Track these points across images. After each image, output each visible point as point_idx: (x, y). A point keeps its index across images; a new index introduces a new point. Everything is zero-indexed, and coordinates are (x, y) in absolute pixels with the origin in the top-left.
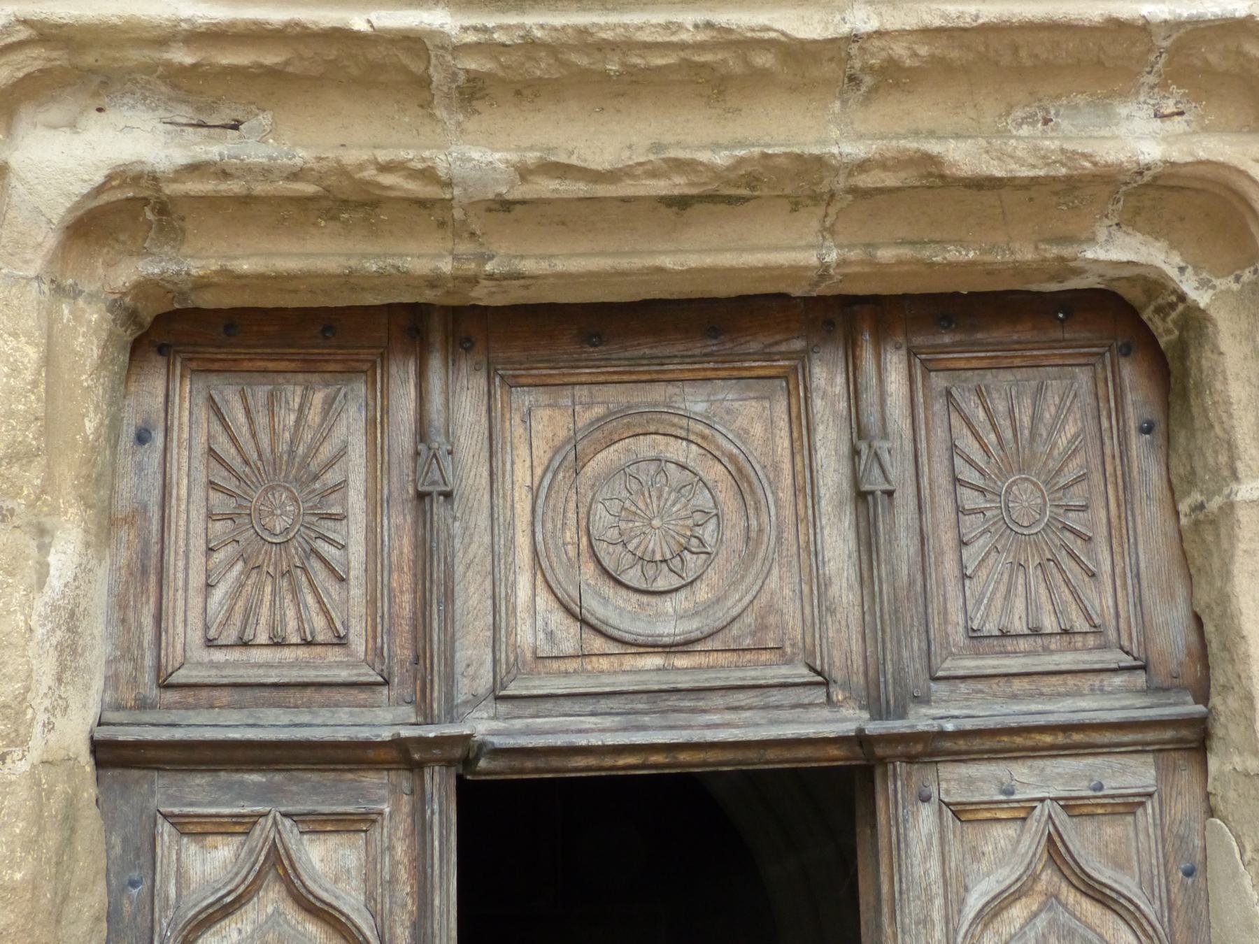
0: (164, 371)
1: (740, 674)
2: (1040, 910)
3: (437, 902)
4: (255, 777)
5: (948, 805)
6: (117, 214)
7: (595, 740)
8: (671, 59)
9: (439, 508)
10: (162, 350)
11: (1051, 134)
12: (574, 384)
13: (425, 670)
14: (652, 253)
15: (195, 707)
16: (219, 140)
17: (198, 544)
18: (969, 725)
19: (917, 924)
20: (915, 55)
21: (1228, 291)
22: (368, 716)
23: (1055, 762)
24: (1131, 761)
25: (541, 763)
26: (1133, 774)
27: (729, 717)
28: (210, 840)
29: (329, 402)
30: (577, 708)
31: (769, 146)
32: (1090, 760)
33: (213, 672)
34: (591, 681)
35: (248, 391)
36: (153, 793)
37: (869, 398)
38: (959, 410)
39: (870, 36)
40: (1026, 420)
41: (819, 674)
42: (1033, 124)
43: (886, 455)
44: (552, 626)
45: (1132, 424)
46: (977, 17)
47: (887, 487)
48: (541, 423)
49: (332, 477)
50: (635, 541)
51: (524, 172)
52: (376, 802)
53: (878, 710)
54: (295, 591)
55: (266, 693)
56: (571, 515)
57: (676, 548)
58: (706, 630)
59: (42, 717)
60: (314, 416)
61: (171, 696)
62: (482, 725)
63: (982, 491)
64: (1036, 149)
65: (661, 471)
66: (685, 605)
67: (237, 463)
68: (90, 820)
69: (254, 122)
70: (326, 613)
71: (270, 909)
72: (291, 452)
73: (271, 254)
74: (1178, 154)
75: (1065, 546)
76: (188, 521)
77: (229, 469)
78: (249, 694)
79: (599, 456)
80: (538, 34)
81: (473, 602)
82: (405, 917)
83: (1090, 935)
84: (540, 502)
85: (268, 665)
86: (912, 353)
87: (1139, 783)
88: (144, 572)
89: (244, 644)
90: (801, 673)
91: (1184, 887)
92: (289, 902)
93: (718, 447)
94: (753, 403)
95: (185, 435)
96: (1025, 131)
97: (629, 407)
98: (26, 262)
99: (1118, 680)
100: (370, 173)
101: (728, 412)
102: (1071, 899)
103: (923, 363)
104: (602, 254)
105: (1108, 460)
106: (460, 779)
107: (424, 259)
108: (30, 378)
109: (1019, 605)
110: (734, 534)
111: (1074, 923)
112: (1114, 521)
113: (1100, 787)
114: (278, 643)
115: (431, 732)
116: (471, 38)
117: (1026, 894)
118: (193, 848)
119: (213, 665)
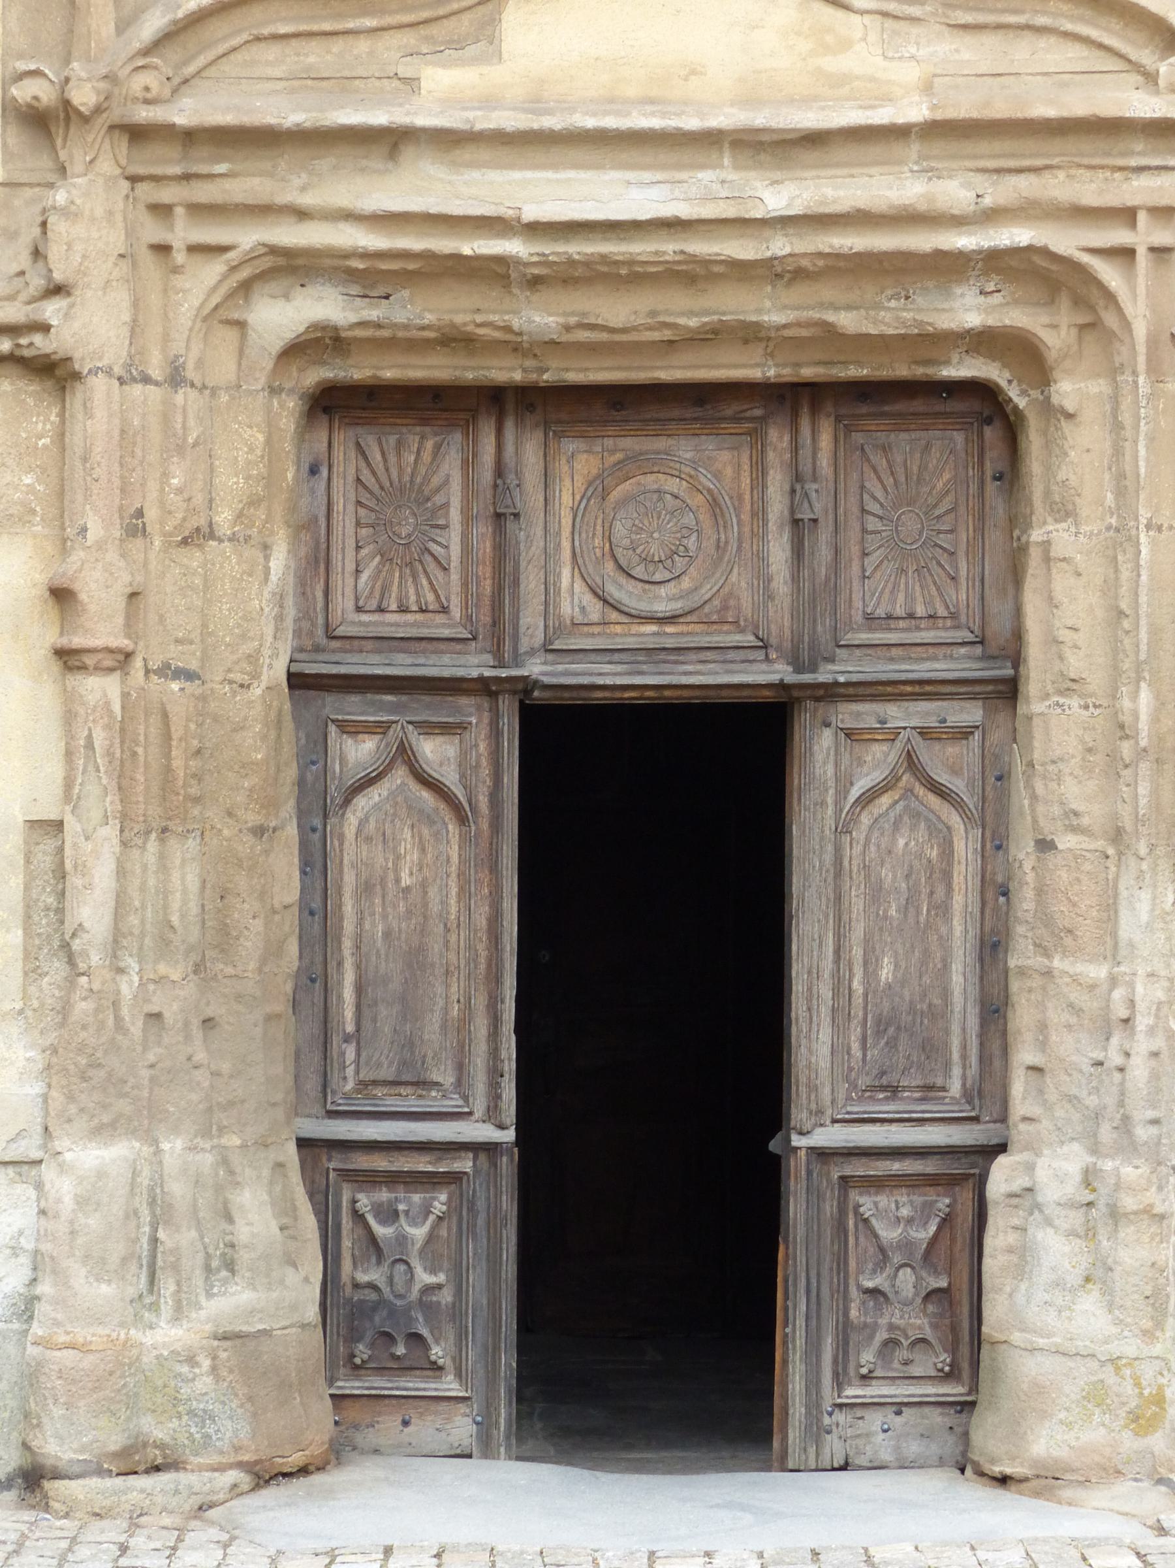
0: (327, 425)
1: (708, 639)
2: (900, 799)
3: (505, 780)
4: (389, 698)
5: (842, 729)
6: (321, 342)
7: (609, 681)
8: (660, 268)
9: (510, 525)
10: (326, 410)
11: (910, 306)
12: (603, 436)
13: (499, 631)
14: (653, 368)
15: (350, 651)
16: (377, 306)
17: (351, 543)
18: (855, 678)
19: (816, 804)
20: (815, 265)
21: (1037, 399)
22: (462, 660)
23: (915, 703)
24: (968, 705)
25: (574, 694)
26: (969, 713)
27: (700, 667)
28: (361, 736)
29: (438, 447)
30: (599, 659)
31: (724, 314)
32: (939, 703)
33: (362, 629)
34: (609, 641)
35: (383, 440)
36: (324, 706)
37: (805, 453)
38: (868, 460)
39: (785, 256)
40: (915, 469)
41: (762, 640)
42: (898, 299)
43: (814, 495)
44: (585, 603)
45: (989, 474)
46: (851, 248)
47: (812, 516)
48: (580, 462)
49: (439, 499)
50: (642, 547)
51: (568, 328)
52: (467, 716)
53: (798, 670)
54: (415, 577)
55: (395, 643)
56: (599, 528)
57: (669, 553)
58: (687, 609)
59: (267, 661)
60: (426, 456)
61: (335, 644)
62: (535, 668)
63: (881, 518)
64: (898, 318)
65: (660, 499)
66: (674, 591)
67: (376, 488)
68: (289, 724)
69: (399, 295)
70: (435, 591)
71: (399, 782)
72: (412, 482)
73: (404, 367)
75: (934, 558)
76: (344, 526)
77: (371, 493)
78: (385, 644)
79: (619, 488)
80: (577, 257)
81: (532, 586)
82: (485, 789)
83: (931, 816)
84: (578, 519)
85: (397, 625)
86: (838, 419)
87: (970, 719)
88: (317, 561)
90: (750, 639)
91: (995, 788)
92: (411, 777)
93: (700, 483)
94: (726, 452)
95: (341, 469)
96: (893, 304)
97: (641, 454)
98: (256, 379)
99: (963, 650)
100: (470, 328)
101: (709, 458)
102: (921, 793)
103: (845, 427)
104: (619, 368)
105: (971, 498)
106: (521, 702)
107: (506, 371)
108: (259, 454)
109: (901, 597)
110: (709, 545)
111: (921, 808)
112: (971, 540)
113: (945, 721)
114: (403, 610)
115: (504, 673)
116: (535, 259)
117: (890, 788)
118: (350, 741)
119: (361, 624)
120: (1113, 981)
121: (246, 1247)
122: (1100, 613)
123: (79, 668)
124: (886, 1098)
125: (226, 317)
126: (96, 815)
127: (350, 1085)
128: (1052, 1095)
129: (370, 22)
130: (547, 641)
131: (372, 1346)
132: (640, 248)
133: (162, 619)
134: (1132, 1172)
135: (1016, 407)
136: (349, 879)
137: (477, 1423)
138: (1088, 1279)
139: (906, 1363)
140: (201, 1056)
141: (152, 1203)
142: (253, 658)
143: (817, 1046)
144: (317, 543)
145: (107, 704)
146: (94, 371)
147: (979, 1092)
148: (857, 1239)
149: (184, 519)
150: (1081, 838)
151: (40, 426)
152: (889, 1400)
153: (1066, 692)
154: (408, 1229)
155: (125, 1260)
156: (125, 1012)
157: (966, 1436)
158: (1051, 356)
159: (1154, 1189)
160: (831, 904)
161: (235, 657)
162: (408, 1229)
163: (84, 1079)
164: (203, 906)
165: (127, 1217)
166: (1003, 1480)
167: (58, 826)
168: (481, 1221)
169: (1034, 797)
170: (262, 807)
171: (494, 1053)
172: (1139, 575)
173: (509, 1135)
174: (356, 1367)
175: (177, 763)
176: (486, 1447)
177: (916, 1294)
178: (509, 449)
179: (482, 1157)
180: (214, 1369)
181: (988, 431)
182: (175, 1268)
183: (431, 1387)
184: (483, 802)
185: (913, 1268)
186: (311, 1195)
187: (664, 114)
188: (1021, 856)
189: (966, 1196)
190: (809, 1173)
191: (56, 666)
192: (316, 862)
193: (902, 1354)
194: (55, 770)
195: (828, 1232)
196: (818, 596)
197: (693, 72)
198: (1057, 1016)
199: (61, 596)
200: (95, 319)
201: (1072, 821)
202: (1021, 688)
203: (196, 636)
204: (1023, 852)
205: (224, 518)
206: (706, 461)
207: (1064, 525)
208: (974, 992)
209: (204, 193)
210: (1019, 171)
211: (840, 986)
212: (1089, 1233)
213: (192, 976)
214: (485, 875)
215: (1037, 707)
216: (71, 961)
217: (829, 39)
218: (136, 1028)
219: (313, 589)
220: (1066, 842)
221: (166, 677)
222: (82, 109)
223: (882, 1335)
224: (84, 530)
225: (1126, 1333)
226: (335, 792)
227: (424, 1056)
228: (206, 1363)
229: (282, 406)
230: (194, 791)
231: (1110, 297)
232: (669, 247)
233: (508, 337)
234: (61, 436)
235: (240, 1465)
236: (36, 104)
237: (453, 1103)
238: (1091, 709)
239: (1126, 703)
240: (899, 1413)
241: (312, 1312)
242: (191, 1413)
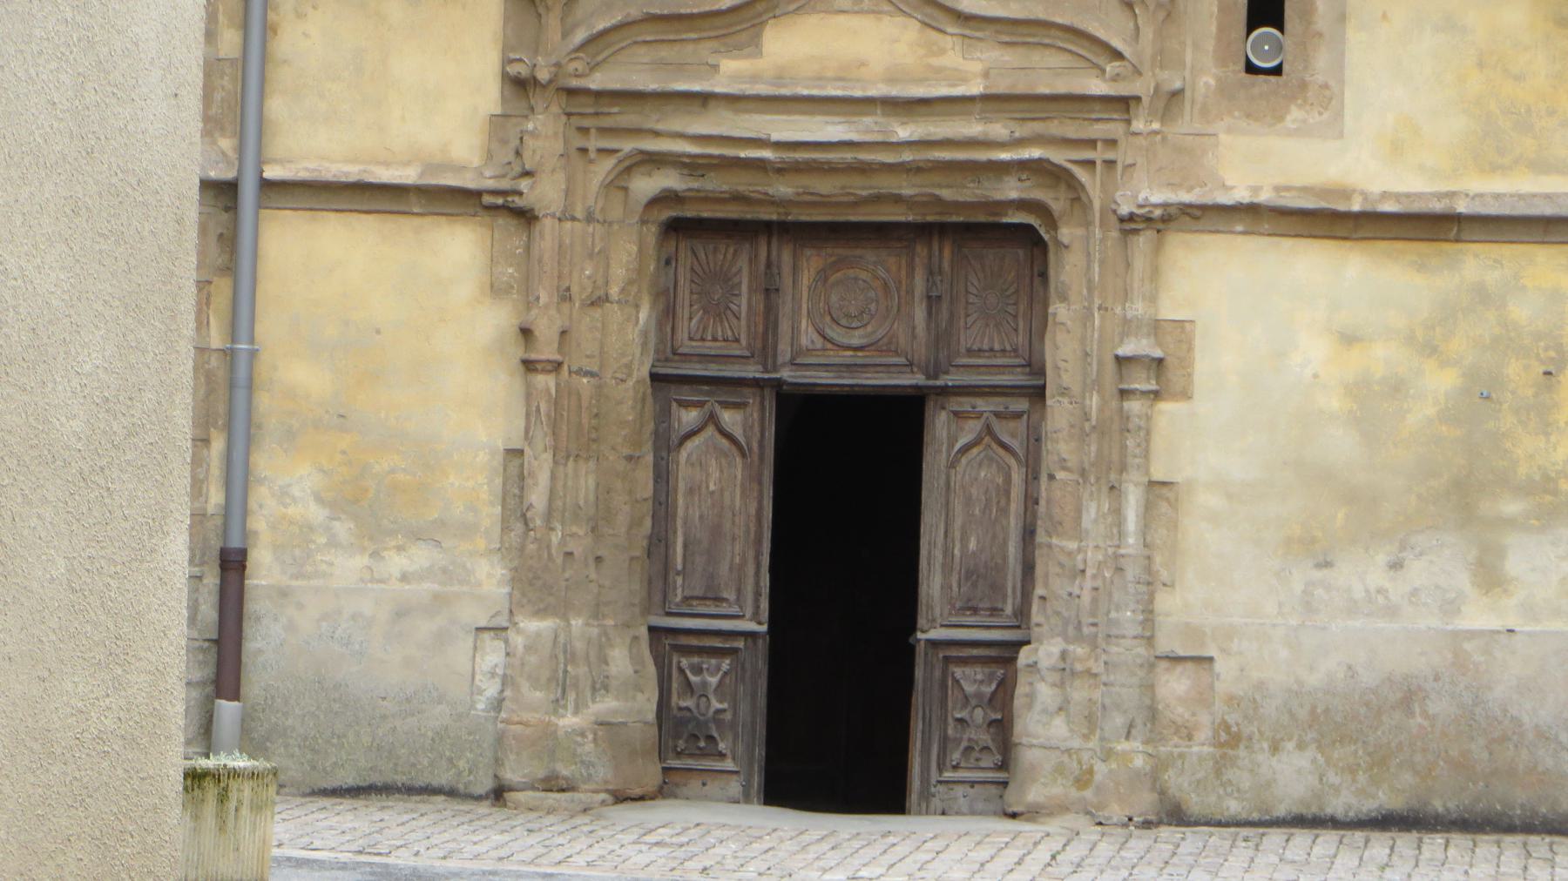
13: (765, 350)
17: (687, 303)
26: (1021, 405)
37: (935, 260)
48: (812, 262)
53: (928, 378)
60: (729, 256)
62: (786, 374)
68: (650, 400)
74: (1024, 195)
89: (703, 339)
90: (902, 360)
114: (715, 339)
115: (766, 376)
120: (1079, 550)
125: (617, 184)
126: (540, 446)
127: (678, 599)
128: (1049, 611)
129: (693, 36)
130: (793, 358)
134: (1079, 650)
136: (682, 486)
138: (1060, 709)
140: (593, 576)
141: (565, 652)
142: (629, 366)
143: (933, 585)
146: (545, 216)
153: (1062, 394)
155: (549, 680)
156: (554, 551)
158: (1056, 215)
163: (531, 584)
167: (521, 452)
168: (748, 674)
171: (757, 583)
173: (764, 628)
175: (585, 421)
176: (746, 798)
178: (774, 253)
180: (595, 740)
182: (576, 686)
183: (718, 765)
184: (755, 445)
187: (844, 88)
191: (522, 368)
192: (663, 475)
193: (975, 754)
194: (521, 423)
195: (936, 687)
196: (941, 338)
199: (526, 333)
203: (597, 353)
204: (1044, 478)
205: (614, 291)
206: (877, 265)
208: (1020, 556)
209: (607, 122)
210: (1033, 119)
211: (948, 552)
212: (1061, 685)
214: (755, 486)
216: (526, 524)
218: (559, 561)
220: (1060, 475)
223: (964, 744)
224: (538, 298)
226: (675, 439)
228: (591, 737)
230: (594, 436)
231: (1083, 186)
232: (849, 156)
234: (528, 249)
235: (607, 791)
237: (735, 610)
241: (651, 716)
242: (582, 762)
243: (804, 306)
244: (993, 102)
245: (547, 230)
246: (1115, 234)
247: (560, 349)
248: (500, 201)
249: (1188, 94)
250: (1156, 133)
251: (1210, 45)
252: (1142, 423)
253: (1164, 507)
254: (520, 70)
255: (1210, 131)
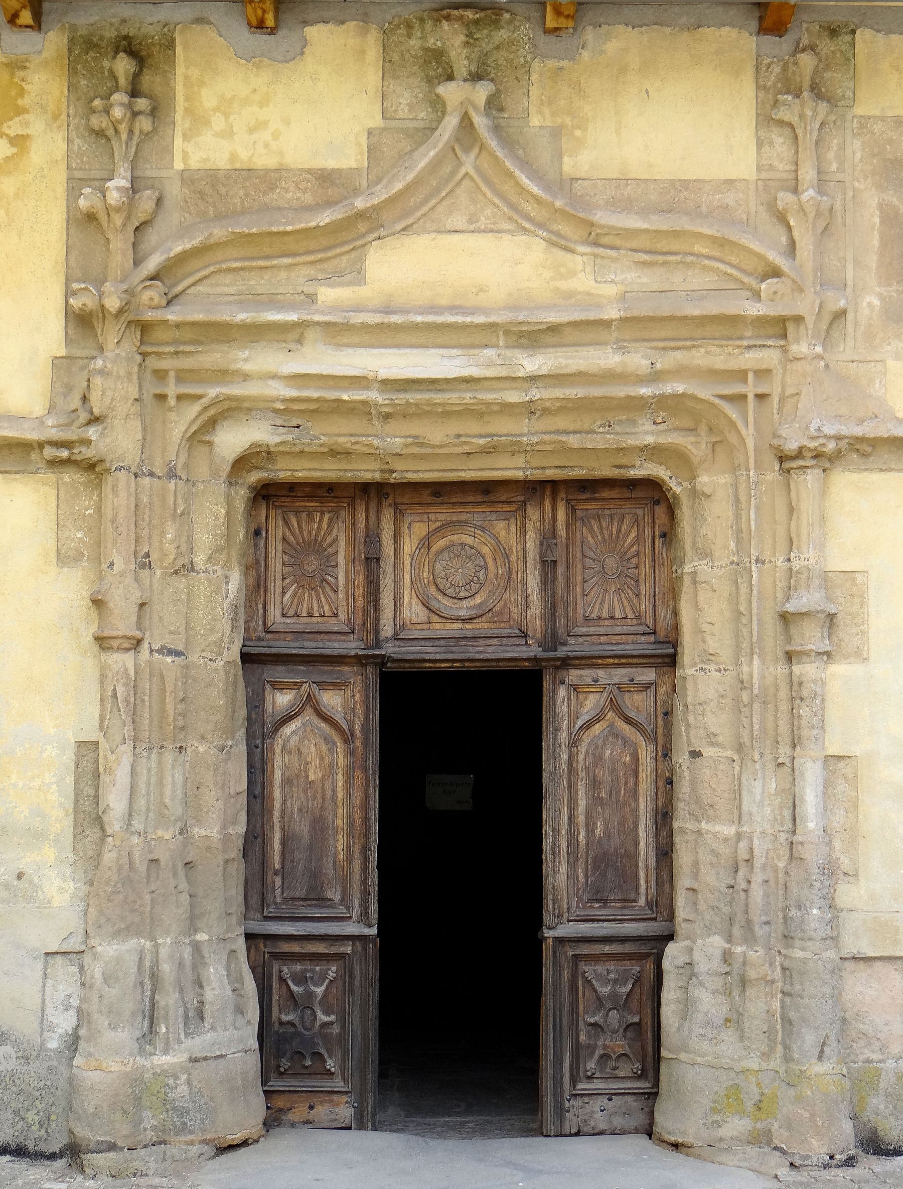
4: (302, 668)
7: (432, 657)
10: (266, 498)
17: (279, 576)
24: (646, 670)
26: (649, 675)
32: (629, 670)
42: (604, 427)
45: (657, 533)
51: (407, 445)
59: (227, 646)
60: (325, 525)
61: (269, 636)
62: (390, 649)
63: (594, 560)
65: (463, 549)
88: (259, 586)
89: (297, 615)
91: (663, 719)
96: (601, 430)
100: (349, 445)
106: (381, 670)
109: (606, 606)
113: (633, 680)
114: (310, 615)
116: (387, 402)
118: (278, 694)
120: (739, 836)
121: (210, 1003)
122: (727, 614)
123: (108, 648)
124: (600, 907)
125: (201, 435)
126: (119, 738)
131: (291, 1059)
132: (452, 397)
133: (161, 618)
135: (674, 493)
136: (278, 775)
137: (355, 1107)
139: (614, 1069)
142: (219, 644)
143: (560, 876)
144: (259, 576)
145: (126, 670)
147: (656, 904)
148: (584, 993)
149: (175, 559)
150: (717, 749)
151: (87, 502)
152: (604, 1092)
154: (312, 988)
155: (133, 1014)
157: (651, 1114)
158: (695, 461)
159: (767, 965)
160: (566, 790)
161: (207, 643)
162: (312, 988)
164: (186, 793)
165: (135, 986)
166: (676, 1146)
169: (688, 725)
170: (223, 733)
171: (365, 881)
172: (752, 591)
173: (374, 931)
174: (281, 1074)
177: (620, 1026)
179: (358, 944)
181: (657, 508)
183: (327, 1085)
185: (618, 1010)
186: (253, 969)
188: (681, 761)
189: (649, 965)
190: (555, 953)
191: (96, 648)
193: (612, 1063)
194: (94, 711)
197: (481, 290)
198: (704, 857)
200: (119, 437)
201: (712, 739)
202: (678, 659)
203: (182, 629)
204: (681, 759)
205: (200, 559)
207: (705, 562)
212: (727, 992)
213: (178, 836)
215: (690, 671)
217: (563, 270)
219: (257, 604)
220: (708, 752)
221: (163, 654)
222: (111, 310)
223: (599, 1052)
224: (112, 564)
225: (752, 1055)
227: (323, 883)
229: (236, 493)
230: (180, 723)
233: (371, 451)
234: (99, 509)
235: (205, 1142)
236: (85, 308)
237: (341, 911)
238: (723, 672)
239: (745, 669)
240: (610, 1099)
242: (174, 1109)
243: (407, 577)
244: (636, 326)
245: (122, 485)
246: (772, 475)
247: (139, 625)
248: (65, 454)
249: (850, 316)
250: (821, 358)
251: (872, 261)
252: (818, 689)
253: (841, 786)
254: (83, 301)
255: (877, 357)
